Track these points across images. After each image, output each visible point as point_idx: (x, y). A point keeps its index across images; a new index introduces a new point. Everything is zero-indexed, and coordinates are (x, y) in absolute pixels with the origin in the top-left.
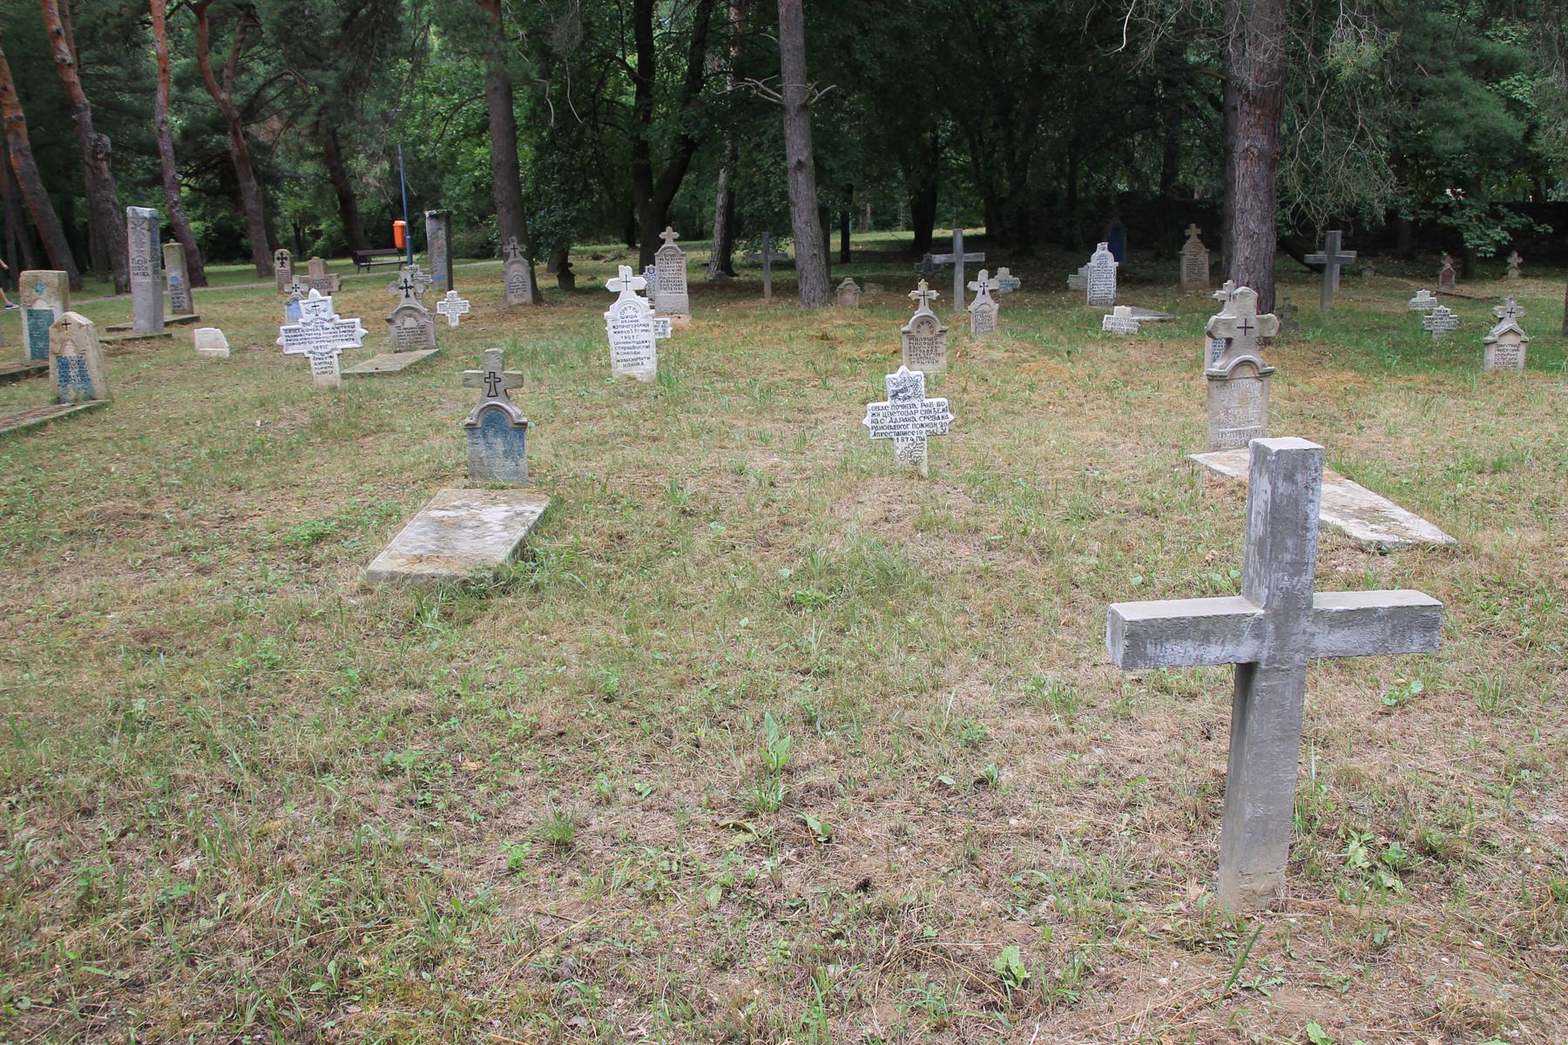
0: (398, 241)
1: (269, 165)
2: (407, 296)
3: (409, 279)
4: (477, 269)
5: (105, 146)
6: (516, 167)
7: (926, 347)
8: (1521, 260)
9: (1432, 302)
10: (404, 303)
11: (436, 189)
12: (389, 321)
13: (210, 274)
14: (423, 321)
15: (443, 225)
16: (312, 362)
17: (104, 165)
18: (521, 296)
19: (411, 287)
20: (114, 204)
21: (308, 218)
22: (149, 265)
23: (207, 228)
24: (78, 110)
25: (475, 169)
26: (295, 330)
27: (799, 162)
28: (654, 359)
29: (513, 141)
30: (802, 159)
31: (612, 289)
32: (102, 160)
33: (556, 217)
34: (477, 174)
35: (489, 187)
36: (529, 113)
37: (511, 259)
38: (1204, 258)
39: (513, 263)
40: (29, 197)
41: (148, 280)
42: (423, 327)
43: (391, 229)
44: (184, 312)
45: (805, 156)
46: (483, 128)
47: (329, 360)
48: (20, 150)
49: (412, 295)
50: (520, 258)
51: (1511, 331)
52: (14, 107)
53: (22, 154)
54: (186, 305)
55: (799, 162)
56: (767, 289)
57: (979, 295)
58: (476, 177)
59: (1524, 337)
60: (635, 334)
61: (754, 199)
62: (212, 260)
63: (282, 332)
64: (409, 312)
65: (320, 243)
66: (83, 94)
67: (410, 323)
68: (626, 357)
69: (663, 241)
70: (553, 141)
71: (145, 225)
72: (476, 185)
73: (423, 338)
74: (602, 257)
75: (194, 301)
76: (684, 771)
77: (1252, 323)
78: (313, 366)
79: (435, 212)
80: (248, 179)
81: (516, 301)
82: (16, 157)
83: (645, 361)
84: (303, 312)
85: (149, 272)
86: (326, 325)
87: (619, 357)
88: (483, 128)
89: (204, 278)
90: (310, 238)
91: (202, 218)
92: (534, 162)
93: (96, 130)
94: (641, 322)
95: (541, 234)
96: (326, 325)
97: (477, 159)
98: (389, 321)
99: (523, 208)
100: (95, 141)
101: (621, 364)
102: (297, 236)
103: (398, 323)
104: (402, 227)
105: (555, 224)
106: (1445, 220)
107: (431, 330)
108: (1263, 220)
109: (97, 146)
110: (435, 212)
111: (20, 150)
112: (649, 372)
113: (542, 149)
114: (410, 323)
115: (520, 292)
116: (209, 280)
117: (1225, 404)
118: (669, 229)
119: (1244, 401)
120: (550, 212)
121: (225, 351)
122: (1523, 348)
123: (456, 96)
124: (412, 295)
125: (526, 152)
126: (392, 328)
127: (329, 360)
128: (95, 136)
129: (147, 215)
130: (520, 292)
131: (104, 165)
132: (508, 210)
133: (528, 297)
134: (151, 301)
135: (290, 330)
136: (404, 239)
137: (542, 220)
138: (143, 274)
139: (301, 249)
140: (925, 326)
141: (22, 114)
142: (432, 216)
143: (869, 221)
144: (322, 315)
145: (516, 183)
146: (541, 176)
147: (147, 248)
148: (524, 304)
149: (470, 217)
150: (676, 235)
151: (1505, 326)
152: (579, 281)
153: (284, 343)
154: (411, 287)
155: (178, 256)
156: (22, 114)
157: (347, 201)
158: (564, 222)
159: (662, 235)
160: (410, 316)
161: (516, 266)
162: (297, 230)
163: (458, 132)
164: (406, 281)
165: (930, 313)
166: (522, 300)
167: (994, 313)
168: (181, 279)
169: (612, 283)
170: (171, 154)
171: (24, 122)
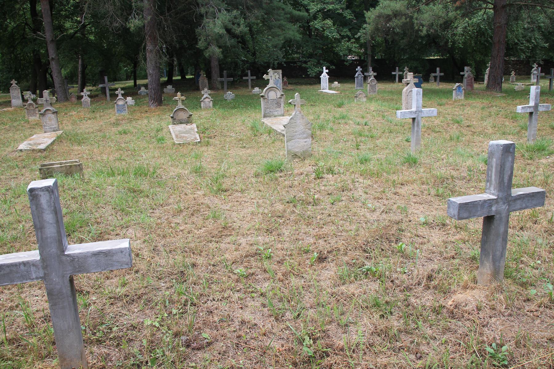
7: (32, 112)
8: (375, 74)
9: (260, 91)
27: (52, 58)
30: (53, 57)
38: (206, 81)
51: (207, 97)
55: (52, 58)
57: (84, 96)
59: (211, 99)
69: (12, 84)
77: (48, 99)
106: (304, 65)
108: (154, 70)
117: (45, 121)
118: (14, 80)
119: (50, 120)
122: (211, 102)
140: (31, 106)
150: (16, 82)
151: (205, 96)
159: (12, 82)
165: (32, 102)
167: (89, 102)
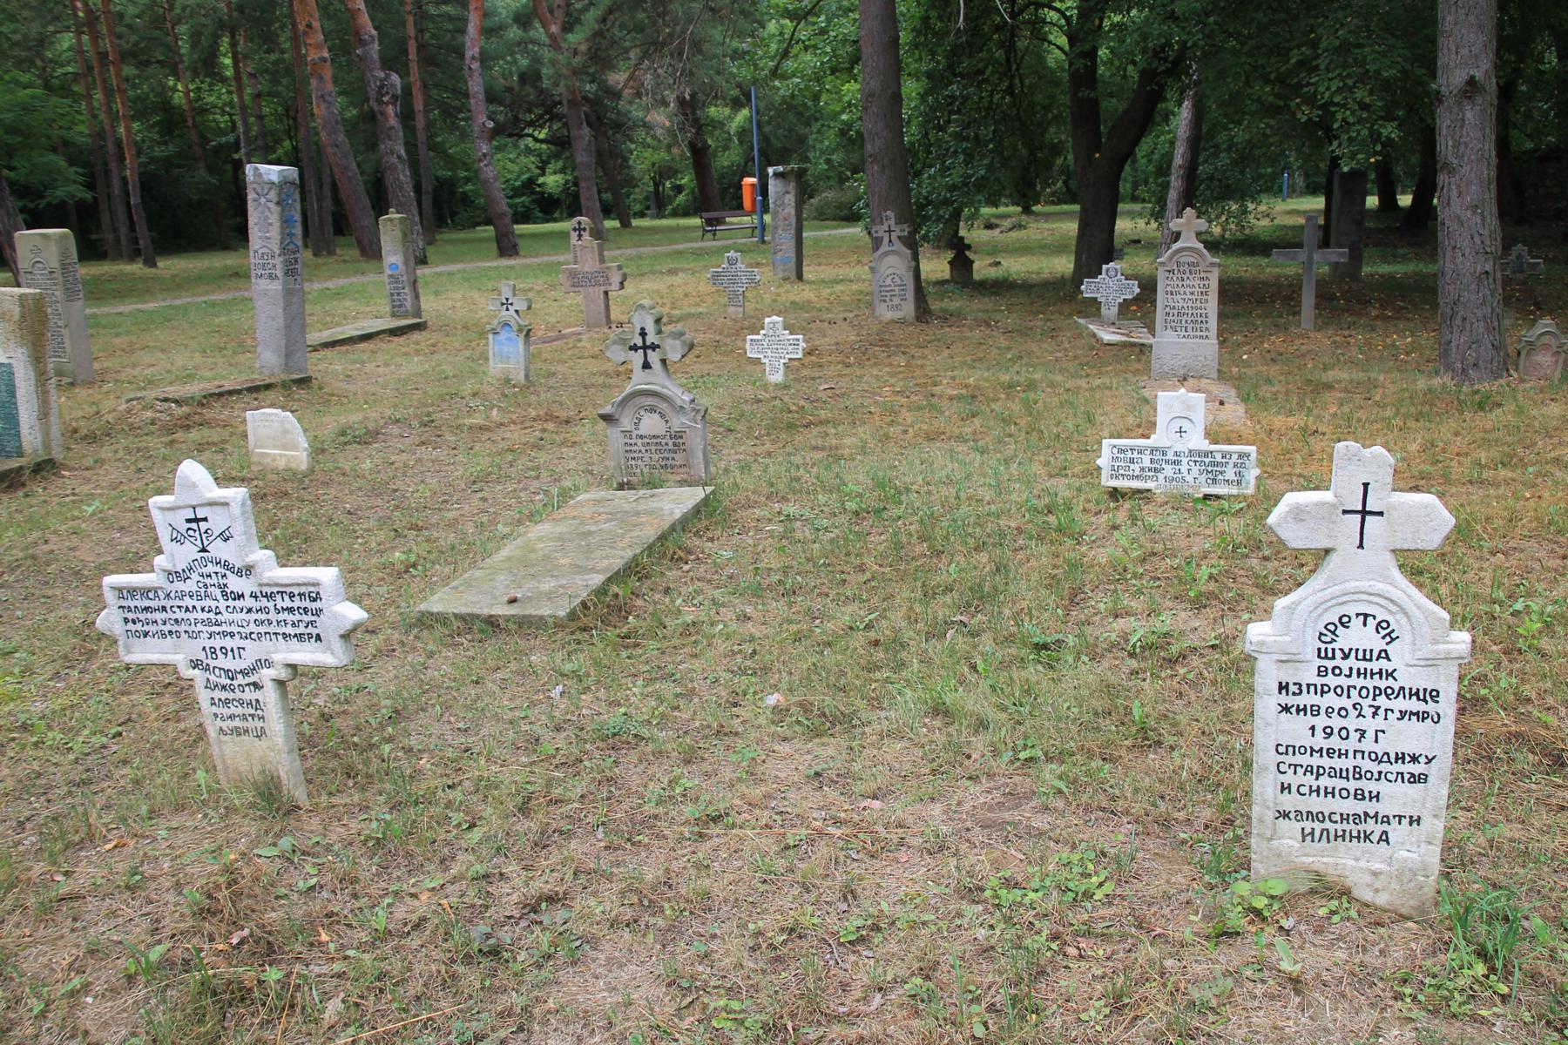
0: (747, 203)
1: (619, 113)
2: (646, 366)
3: (650, 328)
4: (843, 238)
5: (393, 86)
6: (897, 99)
10: (639, 381)
11: (802, 140)
12: (607, 418)
13: (521, 236)
14: (678, 423)
15: (792, 187)
16: (204, 696)
17: (390, 110)
18: (898, 307)
19: (654, 347)
20: (399, 157)
21: (664, 173)
22: (278, 261)
23: (567, 182)
24: (363, 43)
25: (843, 112)
26: (145, 592)
27: (1472, 82)
28: (1435, 826)
29: (895, 69)
30: (1479, 75)
31: (1297, 537)
32: (387, 103)
33: (954, 177)
34: (844, 117)
35: (860, 135)
36: (918, 23)
37: (885, 248)
39: (886, 254)
40: (329, 150)
41: (277, 286)
42: (678, 435)
43: (739, 187)
44: (405, 315)
45: (1483, 69)
46: (855, 59)
47: (249, 695)
48: (322, 96)
49: (656, 365)
50: (898, 246)
52: (318, 47)
53: (325, 101)
54: (408, 304)
55: (1472, 82)
56: (1308, 299)
58: (844, 123)
60: (1370, 724)
61: (1216, 155)
62: (517, 222)
63: (109, 596)
64: (650, 401)
65: (681, 198)
66: (370, 23)
67: (651, 424)
68: (1317, 804)
70: (951, 68)
71: (273, 195)
72: (843, 133)
73: (679, 458)
74: (997, 226)
75: (422, 299)
76: (1099, 973)
78: (205, 704)
79: (781, 168)
80: (580, 127)
81: (889, 315)
82: (318, 104)
83: (1397, 832)
84: (164, 536)
85: (279, 272)
86: (235, 583)
87: (1289, 802)
88: (855, 59)
89: (515, 246)
90: (671, 193)
91: (562, 171)
92: (923, 97)
93: (383, 68)
94: (1405, 679)
95: (929, 203)
96: (235, 583)
97: (846, 99)
98: (607, 418)
99: (906, 164)
100: (381, 80)
101: (1292, 827)
102: (657, 190)
103: (626, 422)
104: (753, 185)
105: (952, 188)
107: (695, 442)
109: (382, 86)
110: (781, 168)
111: (322, 96)
112: (1406, 874)
113: (936, 81)
114: (651, 424)
115: (896, 301)
116: (520, 242)
120: (945, 170)
121: (299, 456)
123: (823, 18)
124: (656, 365)
125: (911, 88)
126: (614, 435)
127: (249, 695)
128: (382, 74)
129: (275, 178)
130: (896, 301)
131: (390, 110)
132: (883, 169)
133: (908, 309)
134: (281, 321)
135: (132, 591)
136: (754, 201)
137: (926, 185)
138: (270, 276)
139: (658, 204)
141: (326, 55)
142: (776, 175)
143: (1300, 182)
144: (218, 550)
145: (896, 123)
146: (932, 122)
147: (275, 232)
148: (902, 322)
149: (842, 172)
152: (982, 268)
153: (118, 629)
154: (654, 347)
155: (398, 233)
156: (326, 55)
157: (700, 156)
158: (965, 184)
160: (652, 410)
161: (891, 259)
162: (656, 185)
163: (822, 63)
164: (643, 334)
166: (897, 315)
168: (402, 267)
169: (1298, 514)
170: (481, 96)
171: (329, 63)
